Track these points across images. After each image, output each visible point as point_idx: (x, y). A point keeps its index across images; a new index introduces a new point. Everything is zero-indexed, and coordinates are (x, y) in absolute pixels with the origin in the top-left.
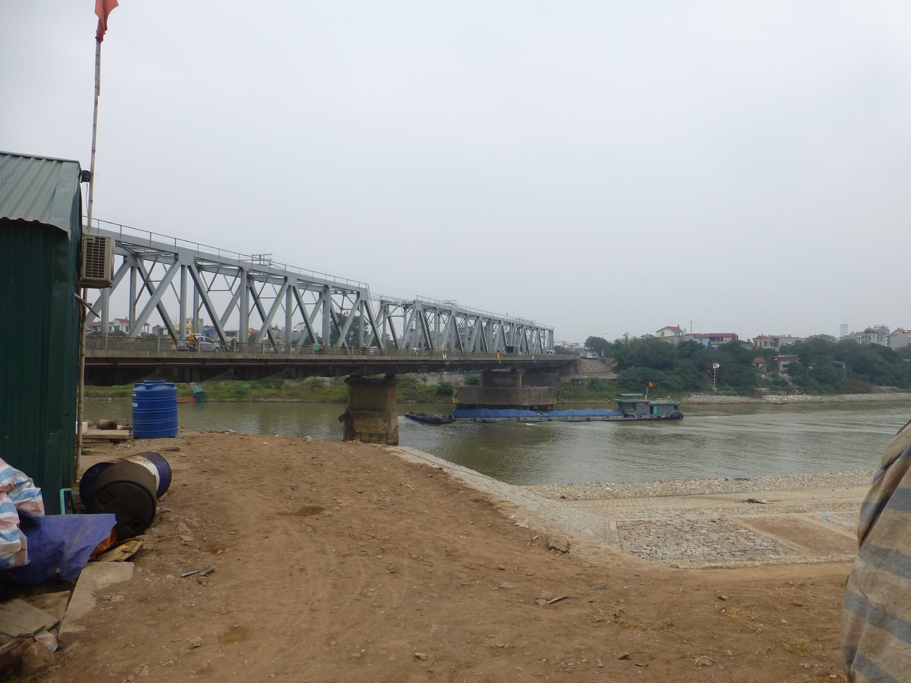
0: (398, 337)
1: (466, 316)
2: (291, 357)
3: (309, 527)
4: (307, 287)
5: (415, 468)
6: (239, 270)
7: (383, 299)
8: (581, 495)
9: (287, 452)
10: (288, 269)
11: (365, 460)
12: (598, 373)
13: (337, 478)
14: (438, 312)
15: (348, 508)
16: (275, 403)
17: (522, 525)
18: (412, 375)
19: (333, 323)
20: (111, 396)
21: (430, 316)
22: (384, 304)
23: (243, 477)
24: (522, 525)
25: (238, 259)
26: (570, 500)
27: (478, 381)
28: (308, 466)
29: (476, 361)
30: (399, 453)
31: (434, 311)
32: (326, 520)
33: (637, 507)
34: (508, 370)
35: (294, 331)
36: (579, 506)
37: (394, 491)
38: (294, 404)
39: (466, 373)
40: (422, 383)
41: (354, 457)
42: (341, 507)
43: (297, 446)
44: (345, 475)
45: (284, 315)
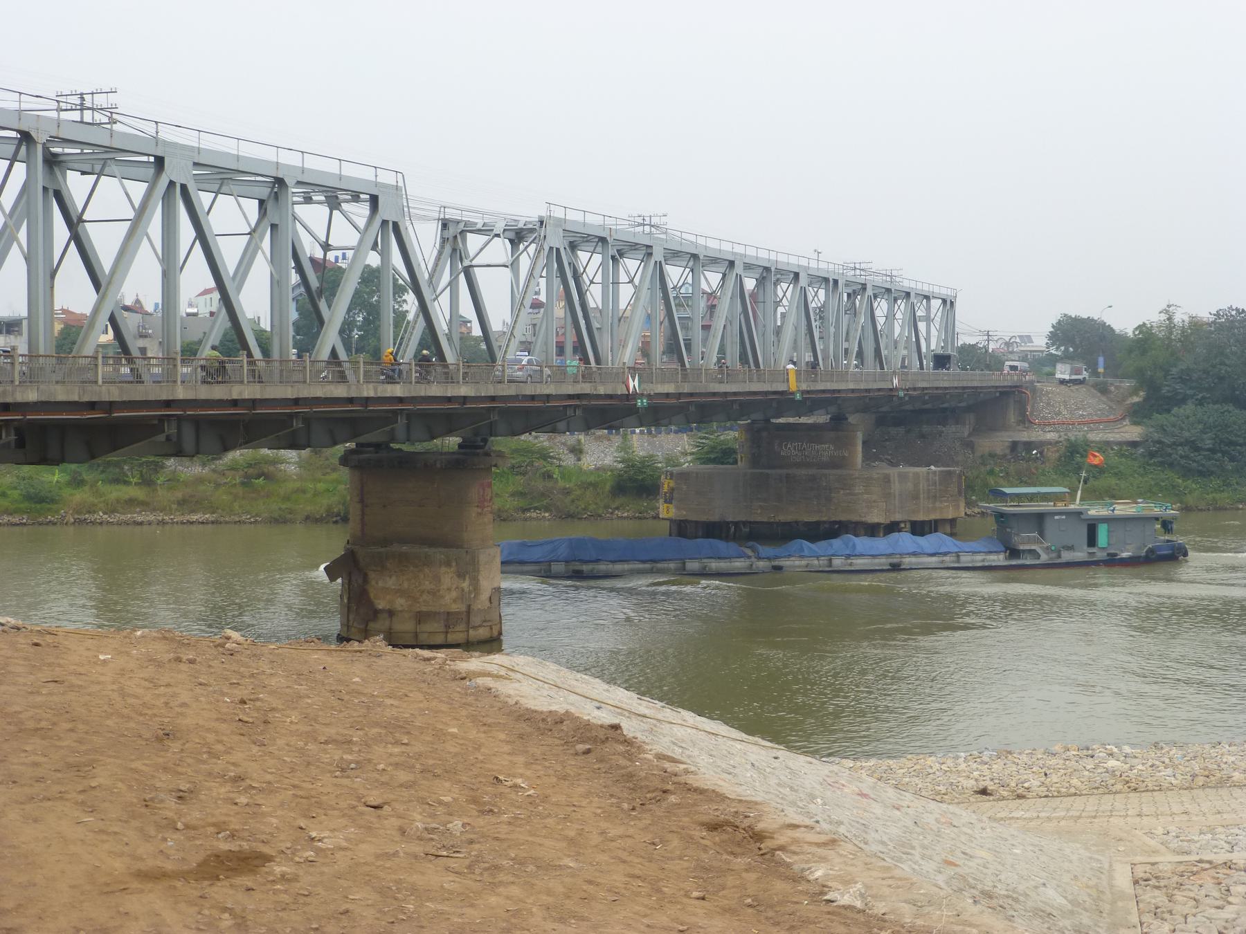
0: (496, 325)
1: (696, 260)
2: (181, 393)
3: (226, 915)
4: (221, 185)
5: (541, 725)
6: (20, 141)
7: (447, 217)
8: (1034, 783)
9: (168, 685)
10: (167, 134)
11: (396, 703)
13: (309, 764)
14: (612, 251)
15: (339, 855)
16: (138, 528)
17: (845, 897)
18: (540, 440)
19: (302, 289)
21: (590, 262)
22: (452, 231)
23: (36, 764)
24: (846, 900)
25: (15, 106)
26: (1004, 798)
27: (734, 451)
28: (223, 727)
29: (726, 394)
30: (498, 677)
31: (599, 249)
32: (276, 892)
33: (1194, 818)
34: (821, 418)
35: (189, 315)
36: (1028, 815)
37: (474, 801)
38: (194, 528)
39: (698, 429)
40: (569, 460)
41: (364, 694)
42: (319, 851)
43: (197, 667)
44: (335, 754)
45: (157, 270)
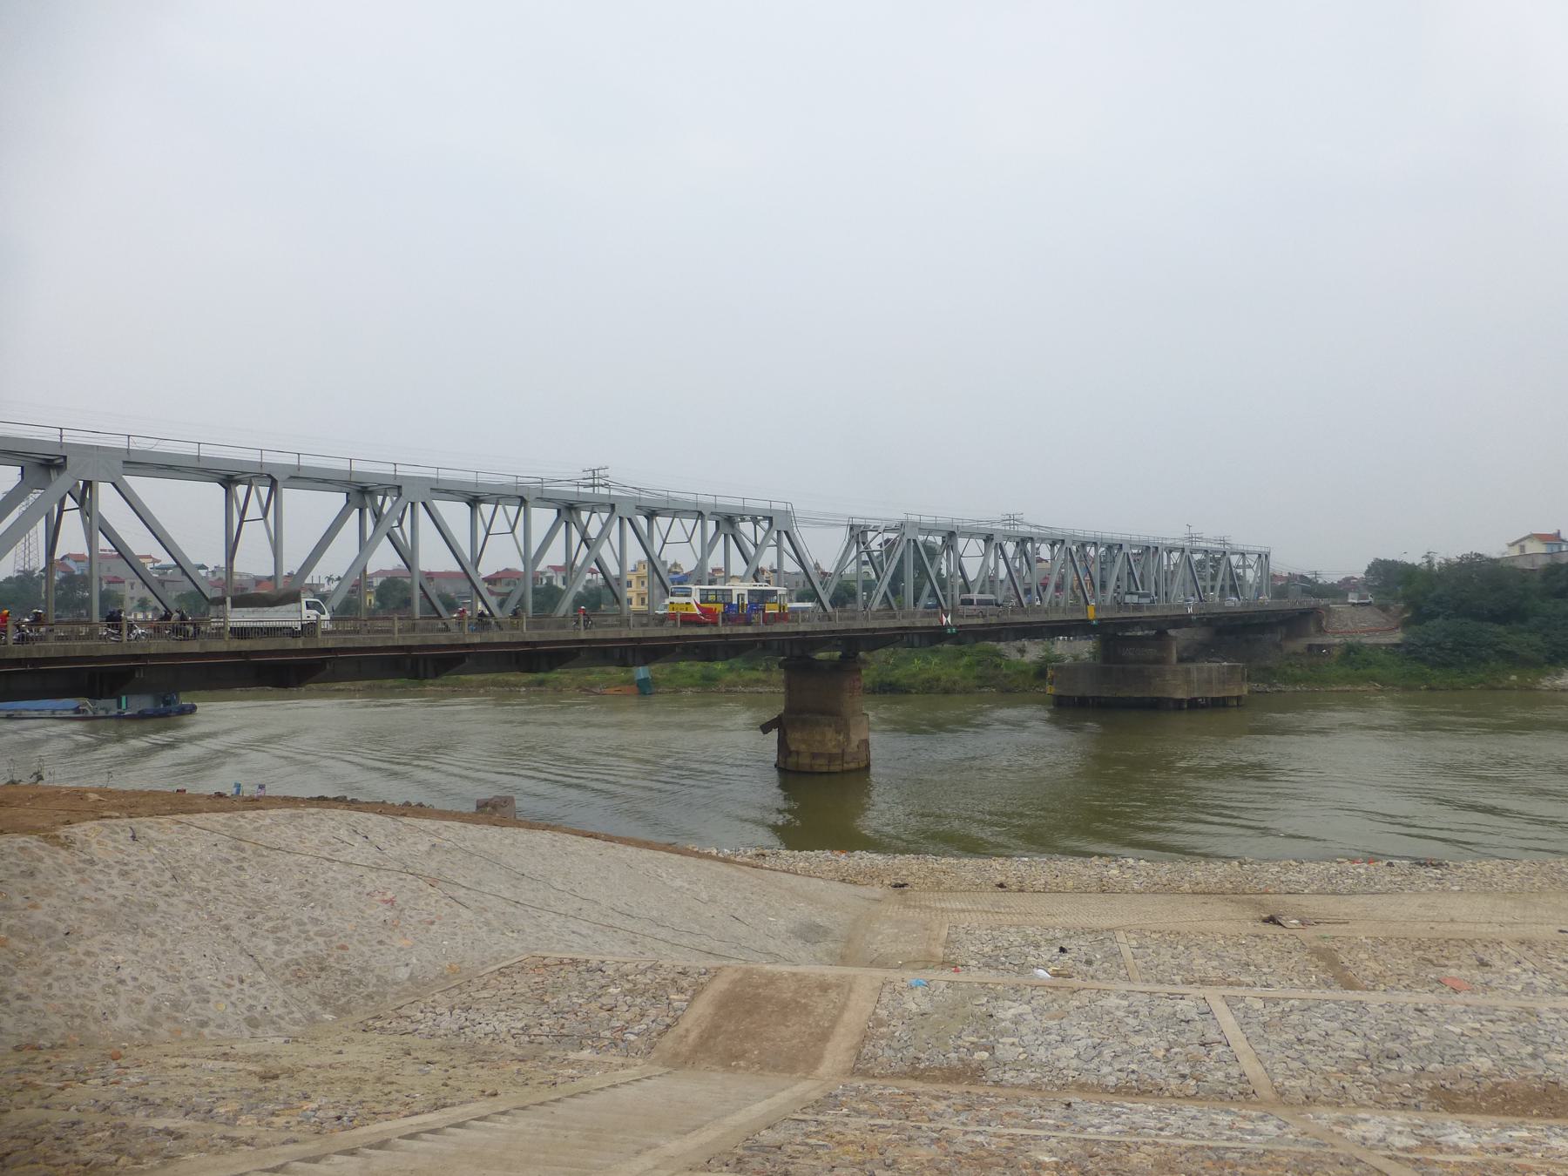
12: (1367, 632)
20: (525, 685)
